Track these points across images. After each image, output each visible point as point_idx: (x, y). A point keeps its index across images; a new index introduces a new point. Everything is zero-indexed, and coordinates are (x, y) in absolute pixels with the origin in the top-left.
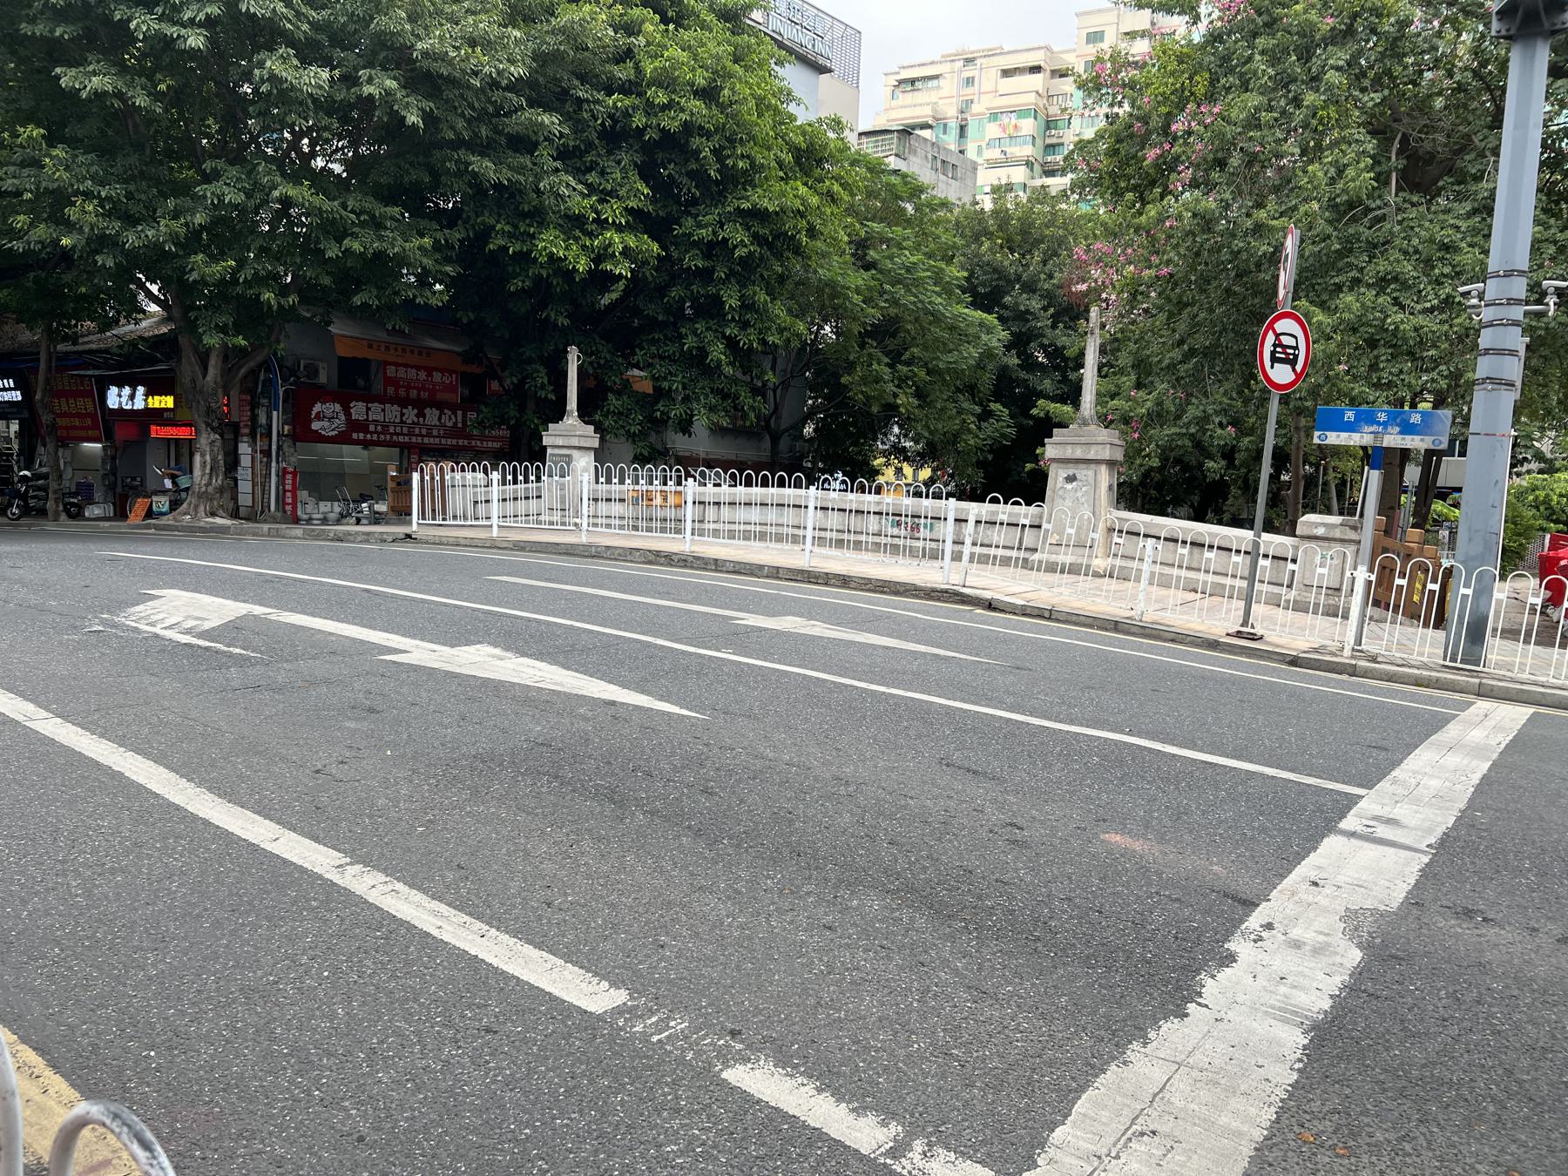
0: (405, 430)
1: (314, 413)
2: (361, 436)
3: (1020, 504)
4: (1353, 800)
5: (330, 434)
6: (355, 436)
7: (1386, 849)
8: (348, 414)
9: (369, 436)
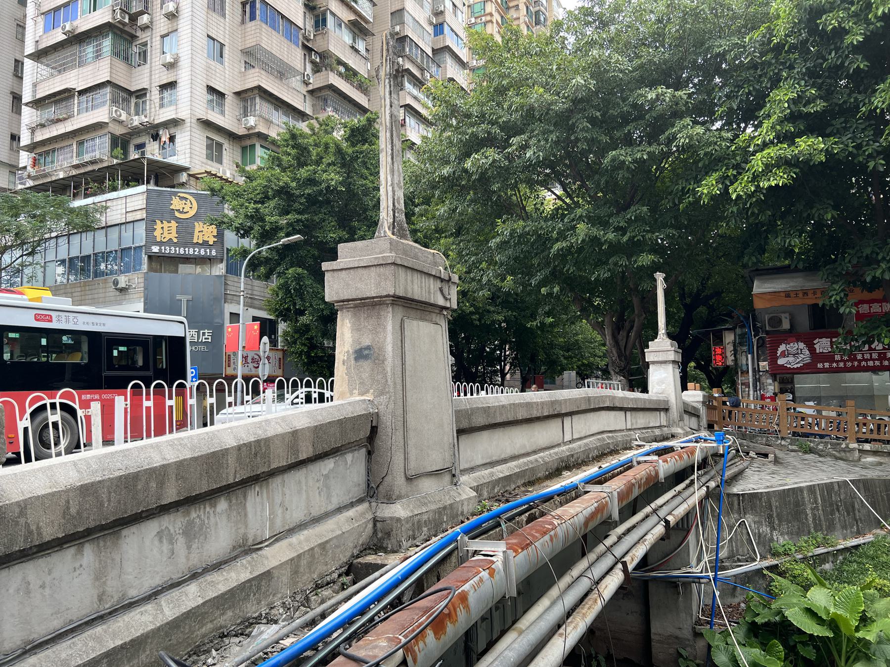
0: (875, 356)
1: (779, 353)
2: (827, 365)
3: (332, 382)
4: (852, 481)
5: (795, 366)
6: (820, 366)
7: (589, 597)
8: (812, 350)
9: (835, 365)
